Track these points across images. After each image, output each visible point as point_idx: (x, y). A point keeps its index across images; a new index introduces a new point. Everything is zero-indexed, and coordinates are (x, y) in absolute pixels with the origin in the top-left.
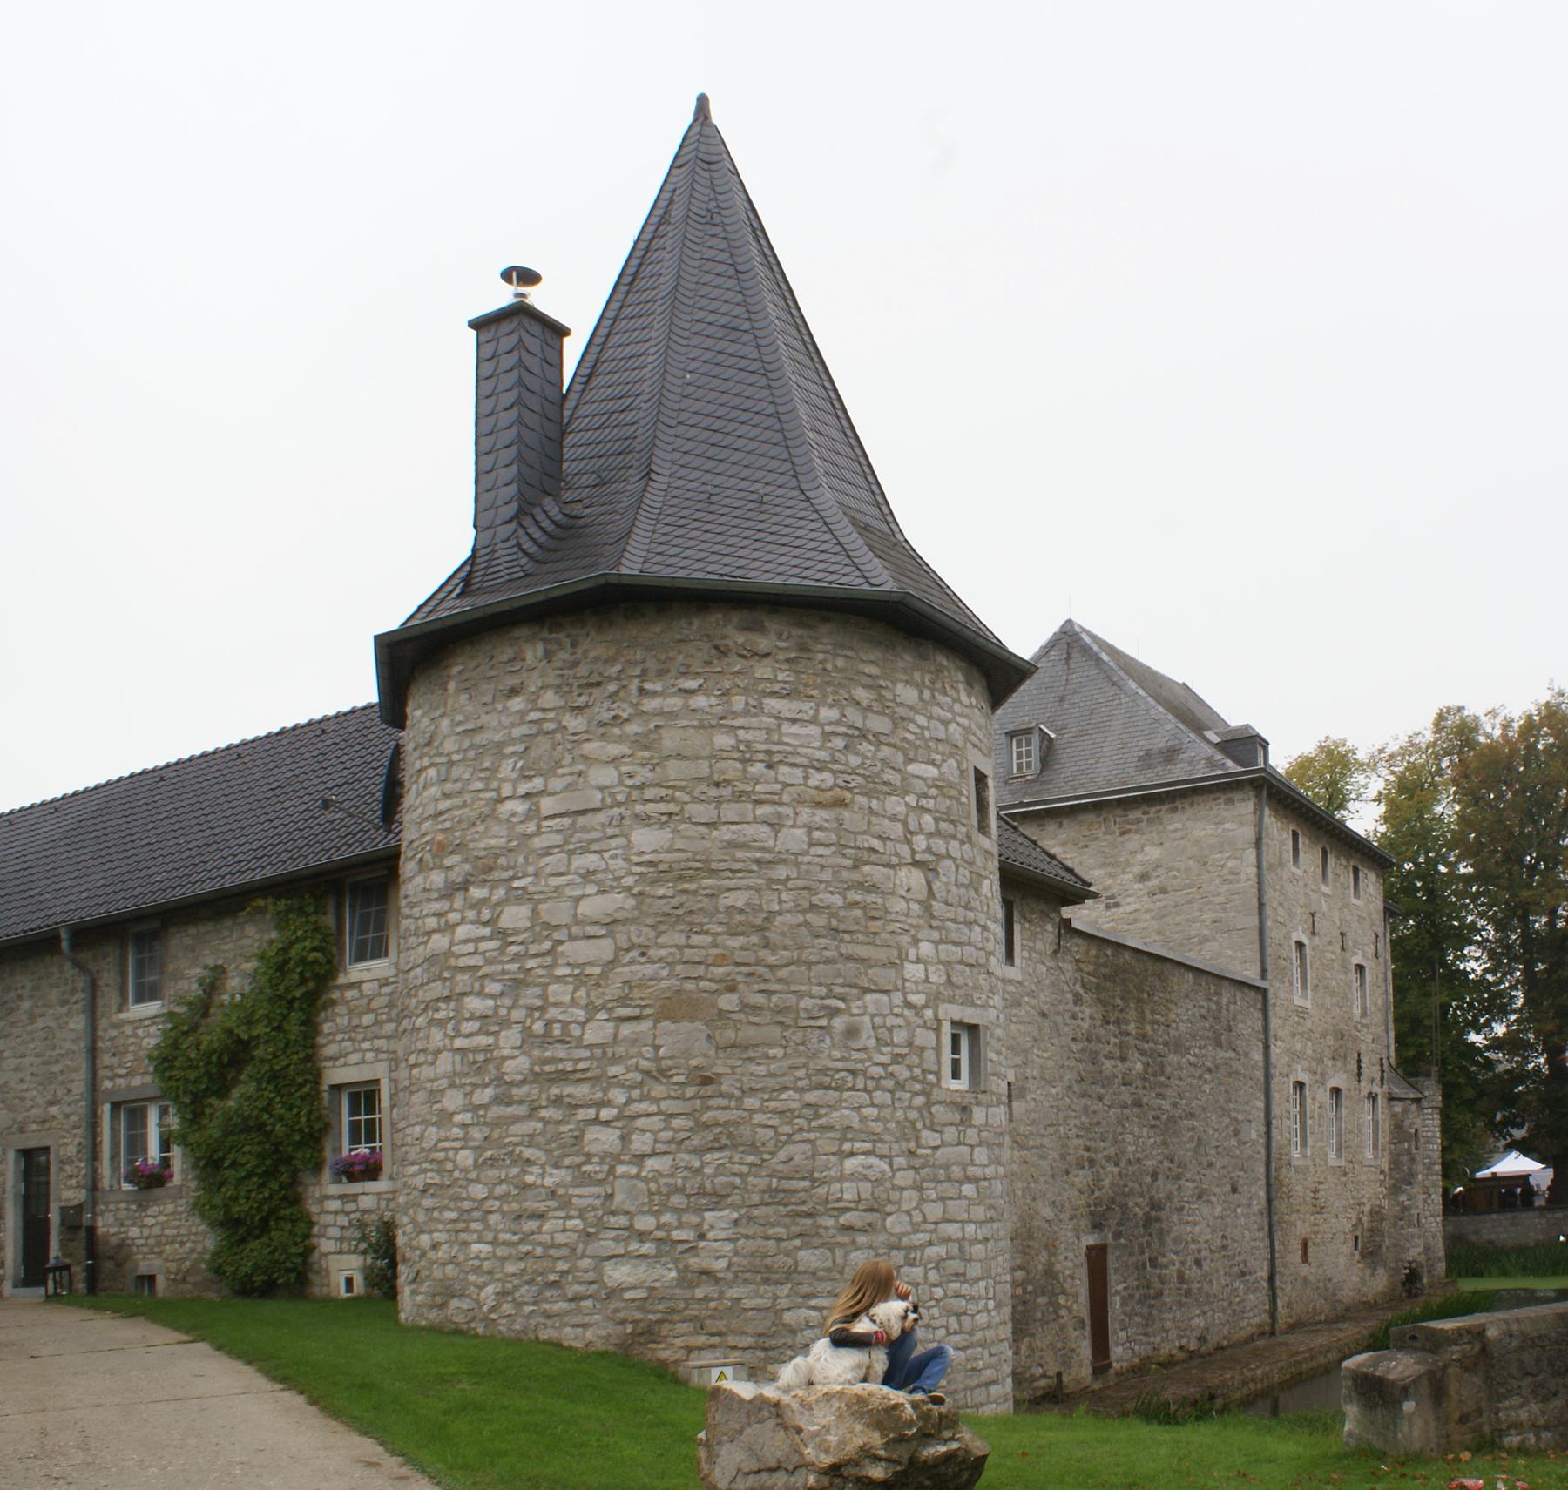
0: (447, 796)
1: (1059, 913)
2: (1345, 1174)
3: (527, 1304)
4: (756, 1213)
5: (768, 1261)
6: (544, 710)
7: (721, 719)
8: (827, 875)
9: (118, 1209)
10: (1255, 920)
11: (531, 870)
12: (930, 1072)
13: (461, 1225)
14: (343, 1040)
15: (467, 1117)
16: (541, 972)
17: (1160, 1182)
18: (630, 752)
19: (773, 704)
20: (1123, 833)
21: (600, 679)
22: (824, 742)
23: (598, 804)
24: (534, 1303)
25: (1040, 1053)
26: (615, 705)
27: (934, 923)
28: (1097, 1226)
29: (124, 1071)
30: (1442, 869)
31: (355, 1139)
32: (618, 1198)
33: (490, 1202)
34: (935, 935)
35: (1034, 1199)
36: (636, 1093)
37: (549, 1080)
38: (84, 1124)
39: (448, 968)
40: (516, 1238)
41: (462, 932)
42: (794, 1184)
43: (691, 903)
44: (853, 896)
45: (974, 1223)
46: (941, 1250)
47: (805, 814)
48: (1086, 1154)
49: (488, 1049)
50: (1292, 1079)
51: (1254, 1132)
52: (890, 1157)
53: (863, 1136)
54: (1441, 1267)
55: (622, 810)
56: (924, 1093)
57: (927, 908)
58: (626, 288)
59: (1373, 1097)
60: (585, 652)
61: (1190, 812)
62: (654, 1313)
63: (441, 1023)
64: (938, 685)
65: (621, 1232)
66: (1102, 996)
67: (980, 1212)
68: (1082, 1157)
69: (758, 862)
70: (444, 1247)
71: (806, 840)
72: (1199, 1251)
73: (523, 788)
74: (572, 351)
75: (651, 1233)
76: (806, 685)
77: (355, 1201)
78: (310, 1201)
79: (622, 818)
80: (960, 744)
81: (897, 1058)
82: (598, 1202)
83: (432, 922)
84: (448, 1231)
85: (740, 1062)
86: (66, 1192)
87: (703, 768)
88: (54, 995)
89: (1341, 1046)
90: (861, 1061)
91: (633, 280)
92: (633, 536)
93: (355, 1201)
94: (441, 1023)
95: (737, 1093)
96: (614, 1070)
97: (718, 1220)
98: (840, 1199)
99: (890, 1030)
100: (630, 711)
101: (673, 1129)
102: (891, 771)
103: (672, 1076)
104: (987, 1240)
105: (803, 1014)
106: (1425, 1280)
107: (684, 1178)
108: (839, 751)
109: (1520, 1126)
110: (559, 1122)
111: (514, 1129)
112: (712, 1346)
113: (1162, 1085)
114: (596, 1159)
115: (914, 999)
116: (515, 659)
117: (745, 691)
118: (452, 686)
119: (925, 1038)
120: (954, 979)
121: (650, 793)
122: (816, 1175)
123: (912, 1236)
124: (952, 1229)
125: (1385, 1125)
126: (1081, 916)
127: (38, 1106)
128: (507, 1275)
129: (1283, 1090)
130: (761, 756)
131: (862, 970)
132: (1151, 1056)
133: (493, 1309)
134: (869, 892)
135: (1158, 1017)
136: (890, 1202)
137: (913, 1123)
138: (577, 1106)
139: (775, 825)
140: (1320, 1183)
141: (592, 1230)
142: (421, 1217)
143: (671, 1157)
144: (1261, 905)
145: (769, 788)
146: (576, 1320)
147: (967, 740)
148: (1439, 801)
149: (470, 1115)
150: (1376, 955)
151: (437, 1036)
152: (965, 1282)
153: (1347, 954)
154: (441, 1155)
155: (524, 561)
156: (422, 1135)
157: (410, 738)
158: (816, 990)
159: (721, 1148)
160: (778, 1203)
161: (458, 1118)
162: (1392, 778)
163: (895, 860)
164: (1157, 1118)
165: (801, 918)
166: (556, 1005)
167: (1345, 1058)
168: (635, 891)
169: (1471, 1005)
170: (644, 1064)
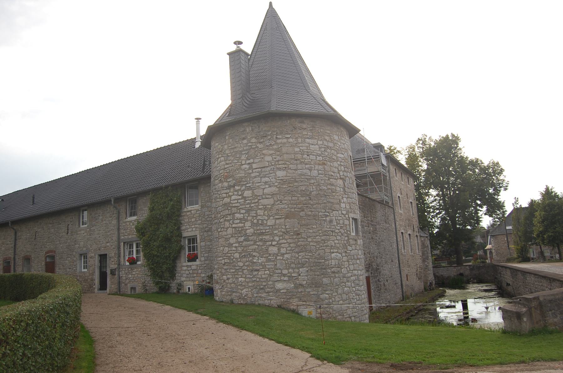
0: (227, 164)
2: (413, 257)
6: (252, 143)
9: (125, 270)
11: (251, 182)
13: (236, 273)
14: (187, 225)
15: (237, 245)
18: (274, 153)
19: (307, 140)
23: (268, 165)
24: (257, 294)
26: (270, 142)
29: (127, 234)
32: (278, 265)
34: (346, 196)
36: (281, 238)
38: (116, 248)
39: (230, 207)
40: (251, 276)
41: (233, 197)
42: (320, 261)
47: (317, 167)
50: (401, 232)
51: (395, 246)
52: (341, 253)
55: (274, 167)
56: (347, 236)
57: (344, 189)
58: (258, 45)
59: (417, 236)
63: (228, 221)
65: (279, 274)
73: (248, 162)
75: (287, 274)
76: (315, 136)
78: (178, 267)
79: (274, 169)
82: (273, 267)
83: (224, 195)
84: (232, 275)
86: (111, 265)
94: (228, 221)
95: (306, 237)
96: (275, 232)
98: (331, 265)
99: (339, 220)
100: (274, 143)
101: (291, 247)
103: (290, 233)
105: (320, 217)
110: (261, 246)
111: (250, 248)
112: (304, 305)
114: (272, 255)
115: (343, 212)
117: (301, 138)
118: (227, 138)
119: (347, 222)
121: (280, 163)
122: (326, 258)
124: (355, 272)
128: (250, 286)
129: (399, 235)
130: (306, 153)
137: (346, 244)
138: (266, 241)
139: (310, 170)
142: (223, 271)
143: (290, 254)
149: (238, 244)
151: (227, 224)
152: (359, 286)
153: (408, 199)
154: (230, 255)
155: (244, 108)
157: (213, 151)
159: (302, 252)
161: (234, 245)
163: (336, 178)
164: (376, 242)
166: (259, 215)
168: (278, 186)
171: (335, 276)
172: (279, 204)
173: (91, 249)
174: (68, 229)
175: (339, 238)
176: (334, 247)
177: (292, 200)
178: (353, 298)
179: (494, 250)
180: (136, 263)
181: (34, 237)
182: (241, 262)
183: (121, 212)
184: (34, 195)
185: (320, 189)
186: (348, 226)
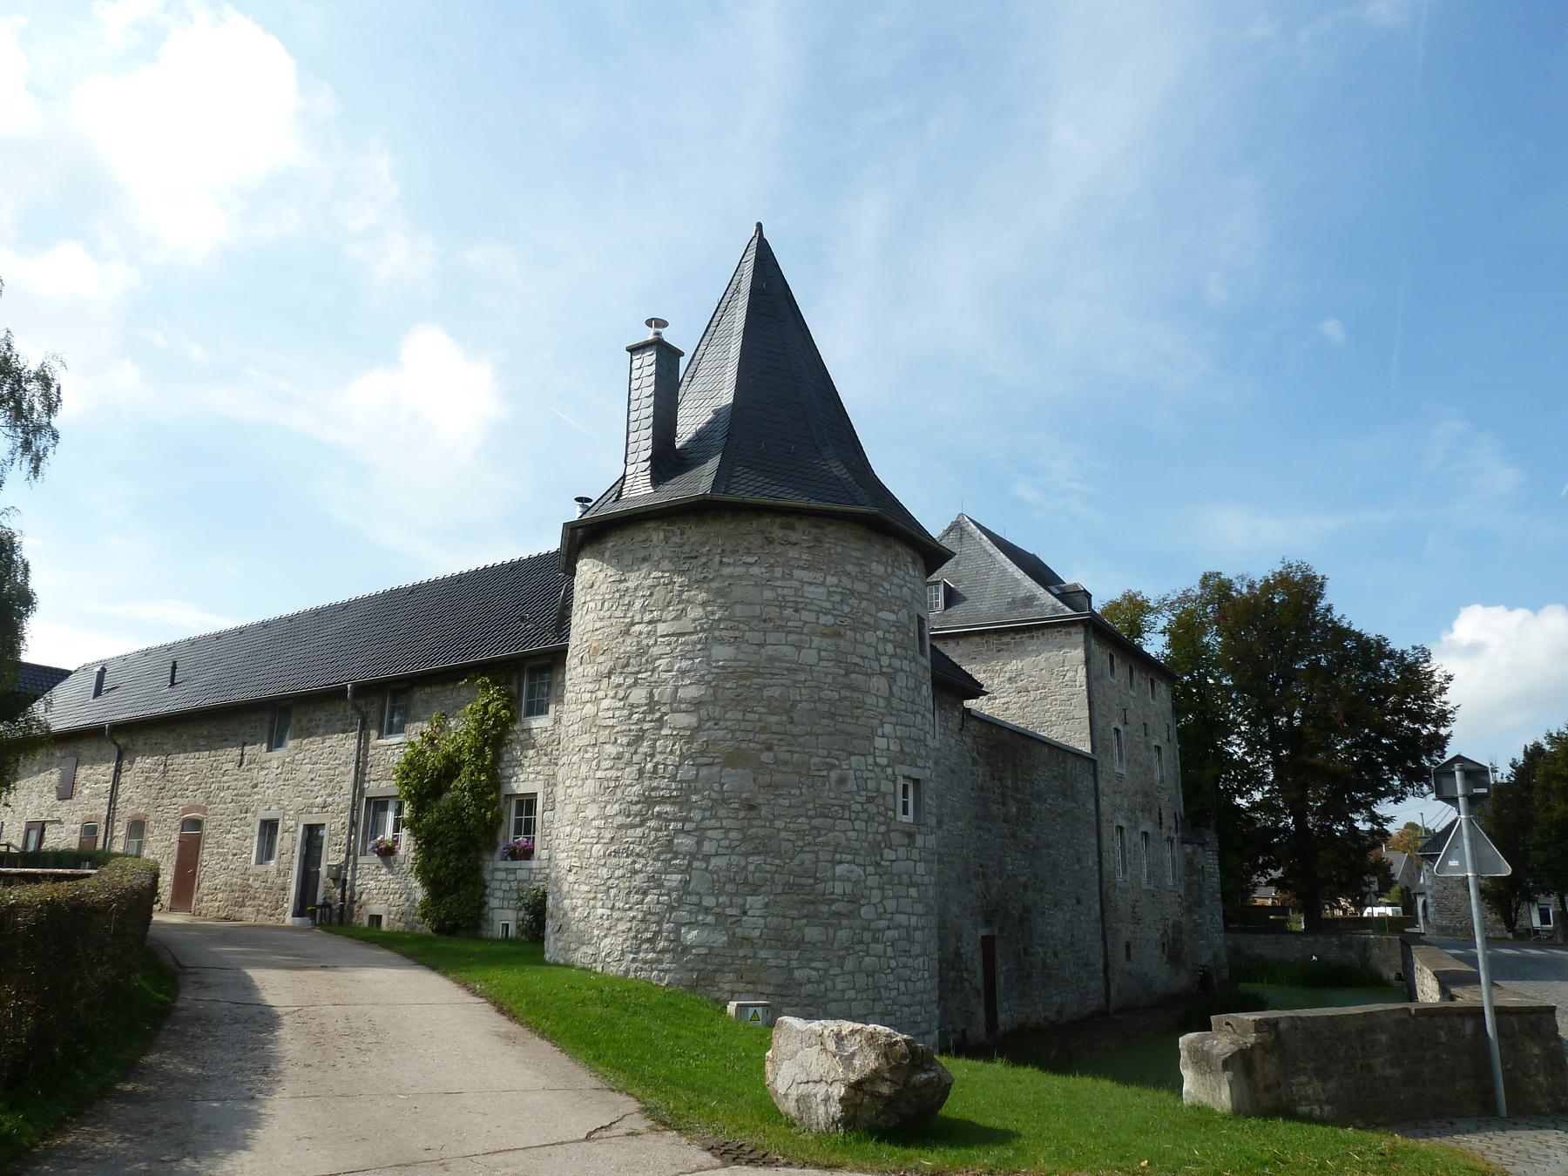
5: (786, 933)
7: (768, 581)
8: (829, 679)
12: (890, 810)
19: (797, 573)
20: (999, 651)
22: (828, 597)
25: (951, 797)
27: (894, 712)
28: (988, 922)
30: (1211, 681)
31: (518, 832)
34: (894, 720)
36: (707, 814)
41: (605, 704)
44: (844, 693)
45: (916, 915)
47: (816, 641)
48: (981, 870)
50: (1115, 824)
51: (1091, 861)
52: (865, 866)
53: (848, 851)
54: (1225, 973)
59: (1169, 839)
61: (1042, 639)
64: (896, 564)
65: (693, 907)
67: (919, 908)
69: (788, 669)
70: (580, 909)
72: (1056, 945)
73: (647, 618)
80: (909, 600)
81: (870, 800)
85: (773, 797)
86: (331, 856)
87: (757, 609)
89: (1147, 803)
90: (848, 800)
97: (755, 902)
98: (833, 893)
99: (866, 780)
102: (868, 616)
103: (731, 803)
104: (924, 928)
106: (1215, 982)
108: (838, 603)
109: (1276, 869)
114: (681, 856)
119: (886, 786)
120: (906, 749)
123: (877, 922)
124: (902, 918)
129: (1108, 832)
130: (791, 604)
131: (849, 739)
133: (608, 955)
134: (854, 691)
135: (1026, 776)
137: (879, 843)
139: (799, 648)
140: (1136, 901)
145: (795, 624)
147: (913, 598)
148: (1206, 635)
150: (1168, 740)
156: (571, 833)
158: (820, 752)
162: (1174, 618)
163: (870, 671)
168: (713, 684)
169: (1235, 777)
170: (714, 795)
171: (840, 924)
172: (708, 729)
175: (859, 825)
176: (846, 847)
177: (744, 720)
178: (886, 987)
179: (1432, 897)
181: (162, 767)
183: (369, 720)
184: (174, 663)
185: (820, 698)
186: (890, 798)
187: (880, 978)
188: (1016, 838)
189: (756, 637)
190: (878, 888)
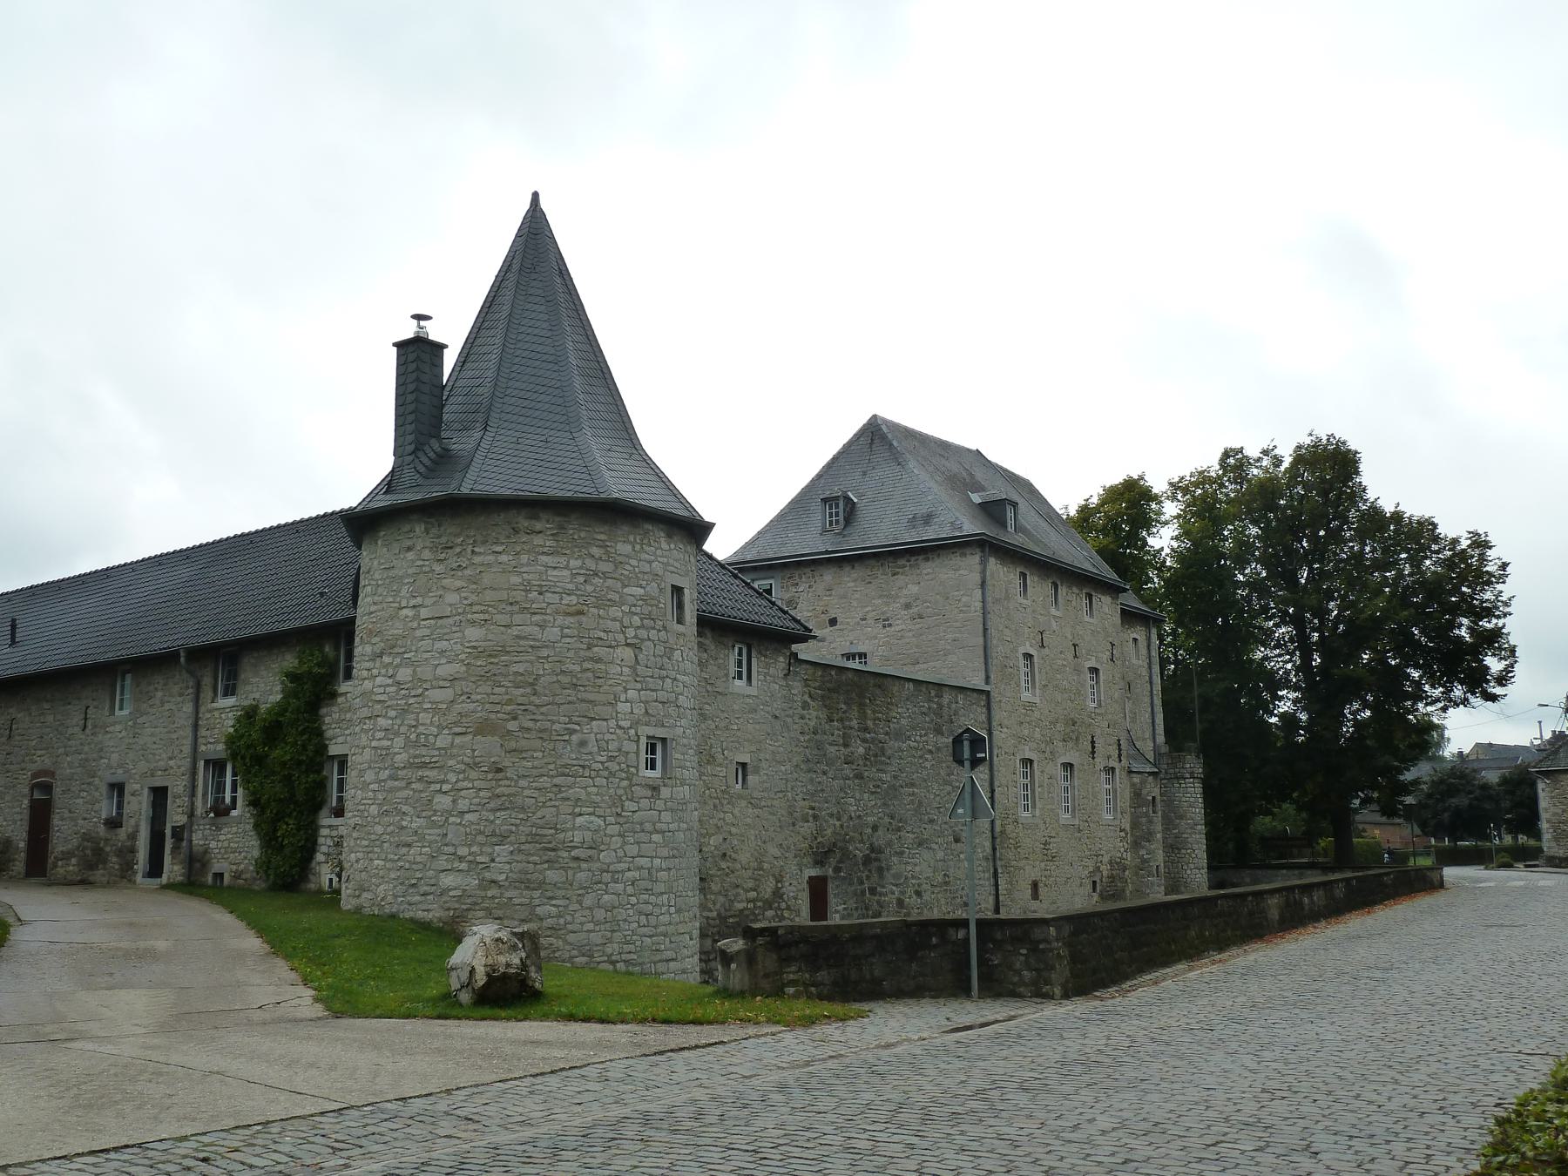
0: (375, 603)
1: (790, 649)
3: (399, 897)
4: (523, 847)
5: (529, 876)
7: (515, 567)
10: (981, 640)
11: (414, 649)
12: (632, 767)
16: (416, 706)
17: (880, 833)
20: (894, 575)
21: (452, 544)
24: (403, 896)
25: (772, 743)
28: (820, 861)
32: (450, 836)
33: (384, 836)
34: (639, 686)
35: (765, 842)
36: (461, 776)
37: (417, 767)
41: (379, 680)
43: (494, 669)
44: (587, 665)
46: (637, 874)
47: (560, 620)
48: (811, 812)
49: (387, 748)
50: (1019, 758)
52: (605, 817)
56: (627, 779)
60: (446, 530)
61: (938, 561)
62: (465, 904)
63: (367, 731)
66: (828, 702)
68: (808, 813)
69: (532, 647)
71: (560, 634)
73: (413, 602)
74: (450, 359)
76: (562, 548)
77: (337, 830)
80: (660, 573)
82: (438, 838)
83: (365, 673)
85: (517, 760)
86: (176, 816)
88: (176, 689)
91: (491, 305)
92: (471, 467)
93: (337, 830)
94: (367, 731)
95: (515, 777)
96: (451, 763)
97: (502, 851)
100: (468, 562)
105: (554, 733)
107: (485, 826)
113: (882, 763)
114: (439, 813)
115: (622, 723)
116: (411, 531)
118: (379, 542)
119: (629, 747)
120: (650, 711)
121: (476, 608)
125: (1125, 795)
126: (804, 651)
127: (163, 760)
130: (536, 588)
132: (872, 742)
133: (382, 899)
136: (603, 843)
137: (620, 797)
139: (542, 627)
141: (435, 855)
142: (352, 843)
144: (985, 630)
146: (424, 907)
151: (364, 740)
160: (536, 842)
163: (614, 643)
165: (555, 679)
166: (423, 725)
167: (1077, 739)
168: (466, 663)
173: (134, 771)
174: (86, 719)
178: (625, 920)
180: (228, 815)
181: (8, 732)
182: (380, 825)
184: (14, 620)
186: (632, 756)
187: (619, 912)
188: (863, 778)
189: (502, 619)
190: (619, 835)
